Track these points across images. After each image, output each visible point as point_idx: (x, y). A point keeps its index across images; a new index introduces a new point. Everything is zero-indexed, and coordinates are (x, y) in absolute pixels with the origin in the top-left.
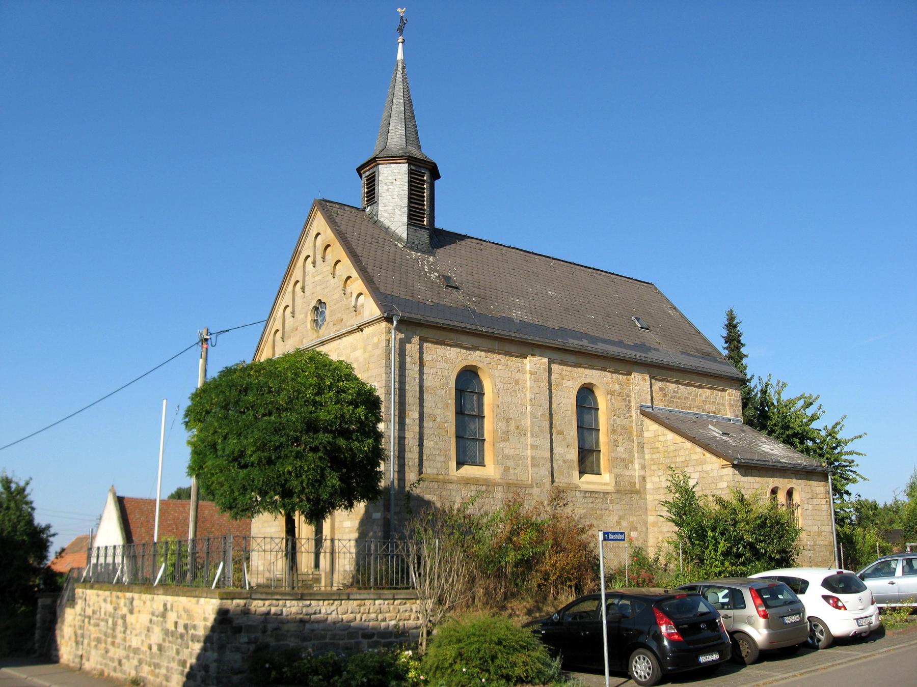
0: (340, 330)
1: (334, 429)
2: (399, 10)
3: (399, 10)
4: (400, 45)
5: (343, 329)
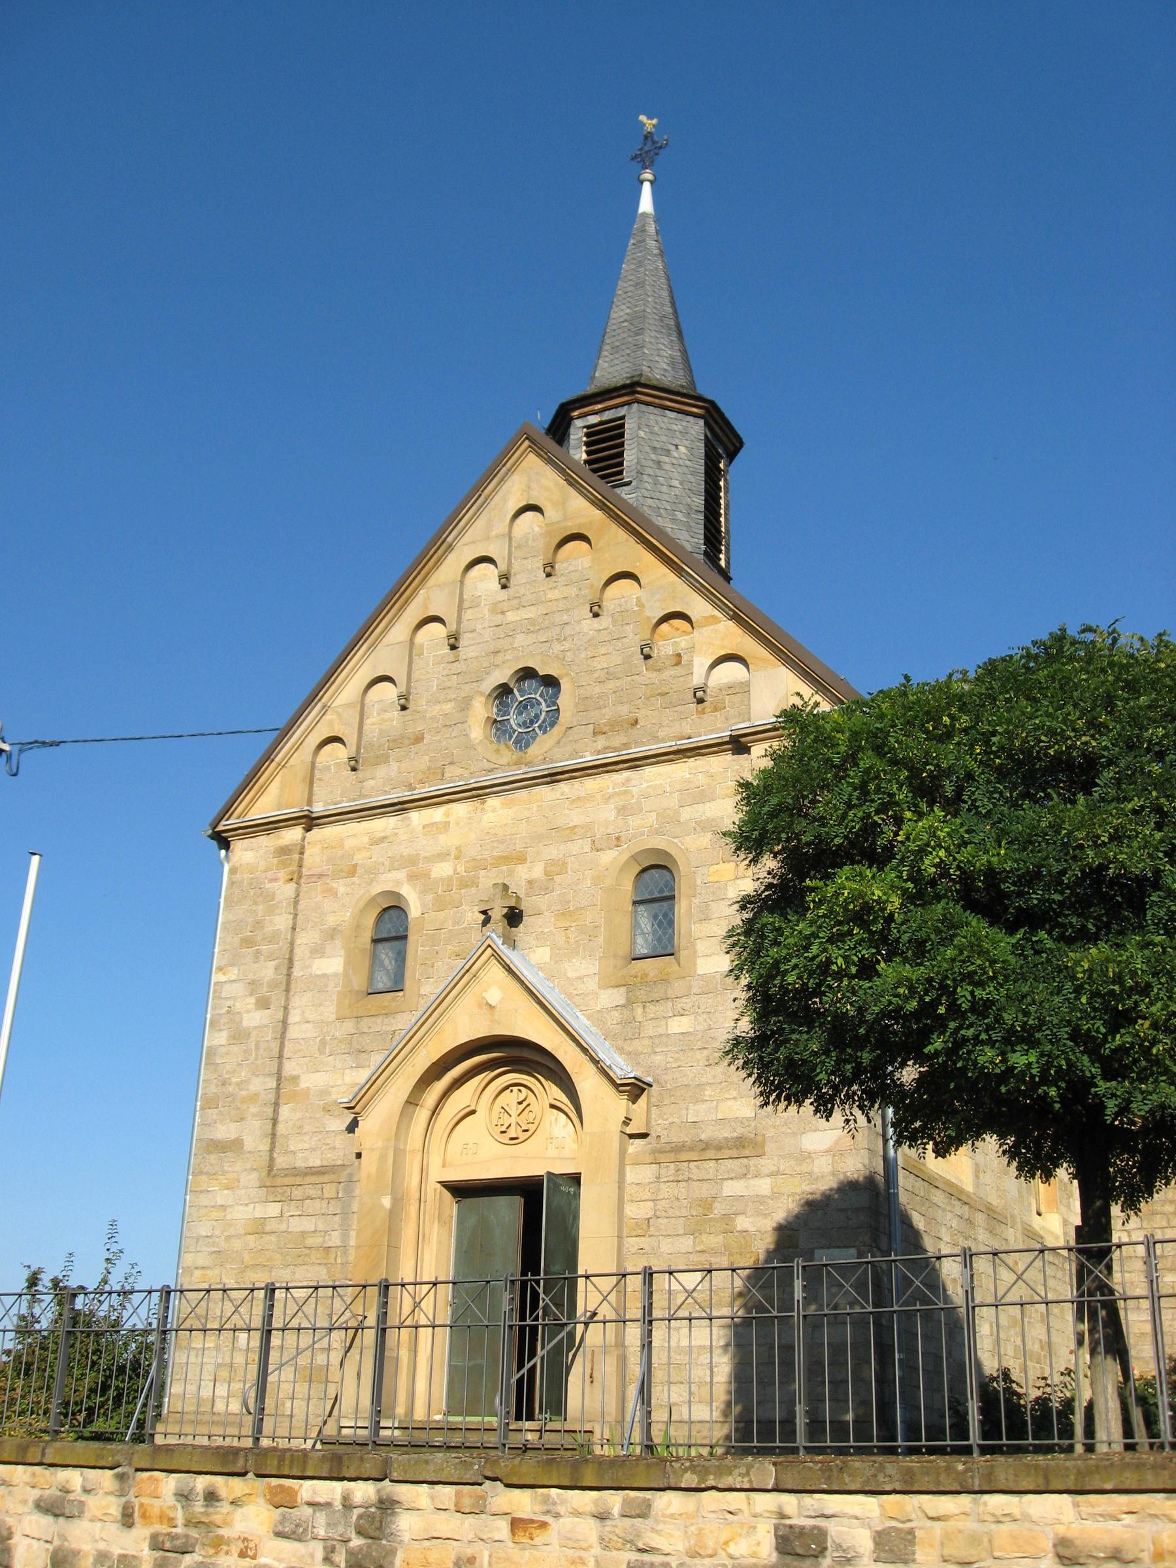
0: (626, 746)
1: (991, 974)
2: (643, 118)
3: (643, 118)
4: (647, 187)
5: (637, 744)
